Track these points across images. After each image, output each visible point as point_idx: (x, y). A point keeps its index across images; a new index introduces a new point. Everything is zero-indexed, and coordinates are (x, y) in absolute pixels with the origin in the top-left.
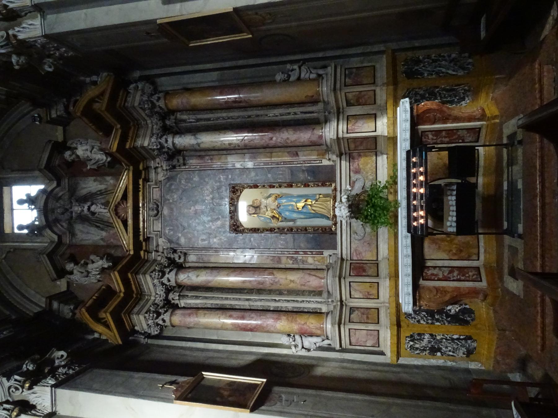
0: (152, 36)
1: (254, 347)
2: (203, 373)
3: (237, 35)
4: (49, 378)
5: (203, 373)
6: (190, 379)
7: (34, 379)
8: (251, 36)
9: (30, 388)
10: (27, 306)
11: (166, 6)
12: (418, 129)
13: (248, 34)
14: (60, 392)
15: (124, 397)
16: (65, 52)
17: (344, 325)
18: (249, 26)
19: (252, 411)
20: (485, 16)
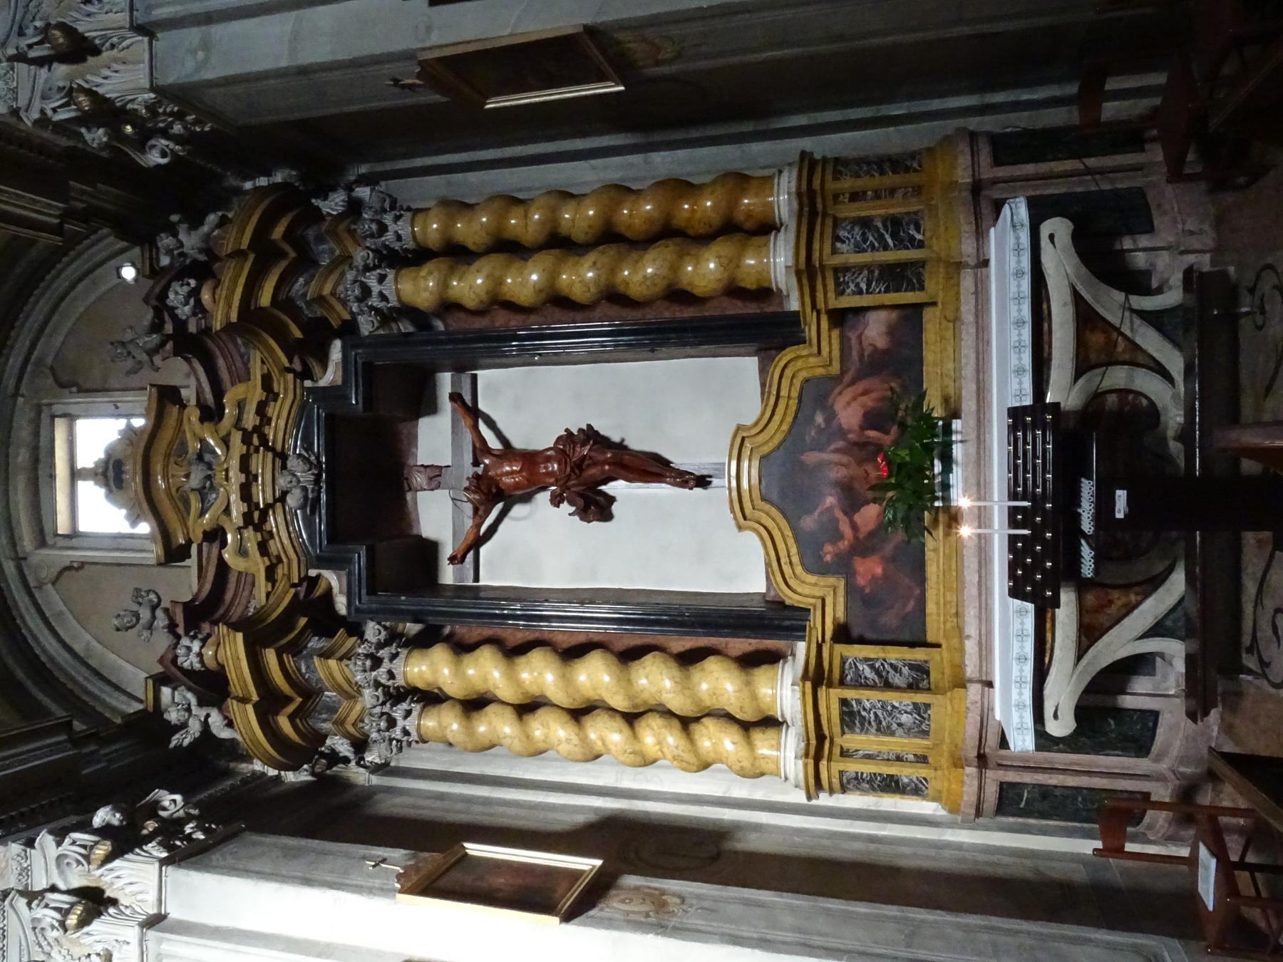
0: (404, 86)
1: (531, 792)
2: (466, 845)
3: (554, 91)
4: (154, 843)
5: (466, 845)
6: (443, 856)
7: (123, 842)
8: (622, 88)
9: (109, 858)
10: (108, 699)
11: (435, 8)
12: (371, 335)
13: (617, 85)
14: (170, 871)
15: (707, 942)
16: (196, 122)
17: (829, 760)
18: (622, 67)
19: (568, 917)
20: (444, 99)
